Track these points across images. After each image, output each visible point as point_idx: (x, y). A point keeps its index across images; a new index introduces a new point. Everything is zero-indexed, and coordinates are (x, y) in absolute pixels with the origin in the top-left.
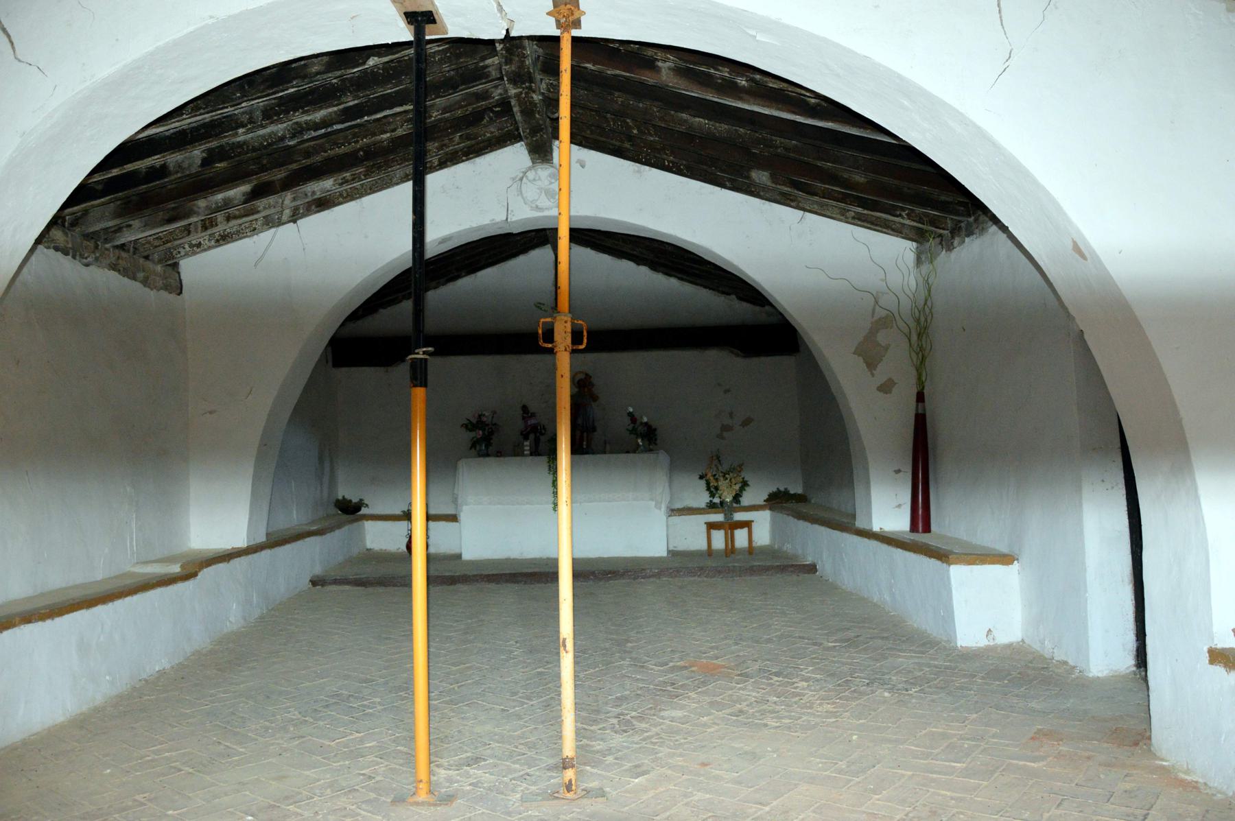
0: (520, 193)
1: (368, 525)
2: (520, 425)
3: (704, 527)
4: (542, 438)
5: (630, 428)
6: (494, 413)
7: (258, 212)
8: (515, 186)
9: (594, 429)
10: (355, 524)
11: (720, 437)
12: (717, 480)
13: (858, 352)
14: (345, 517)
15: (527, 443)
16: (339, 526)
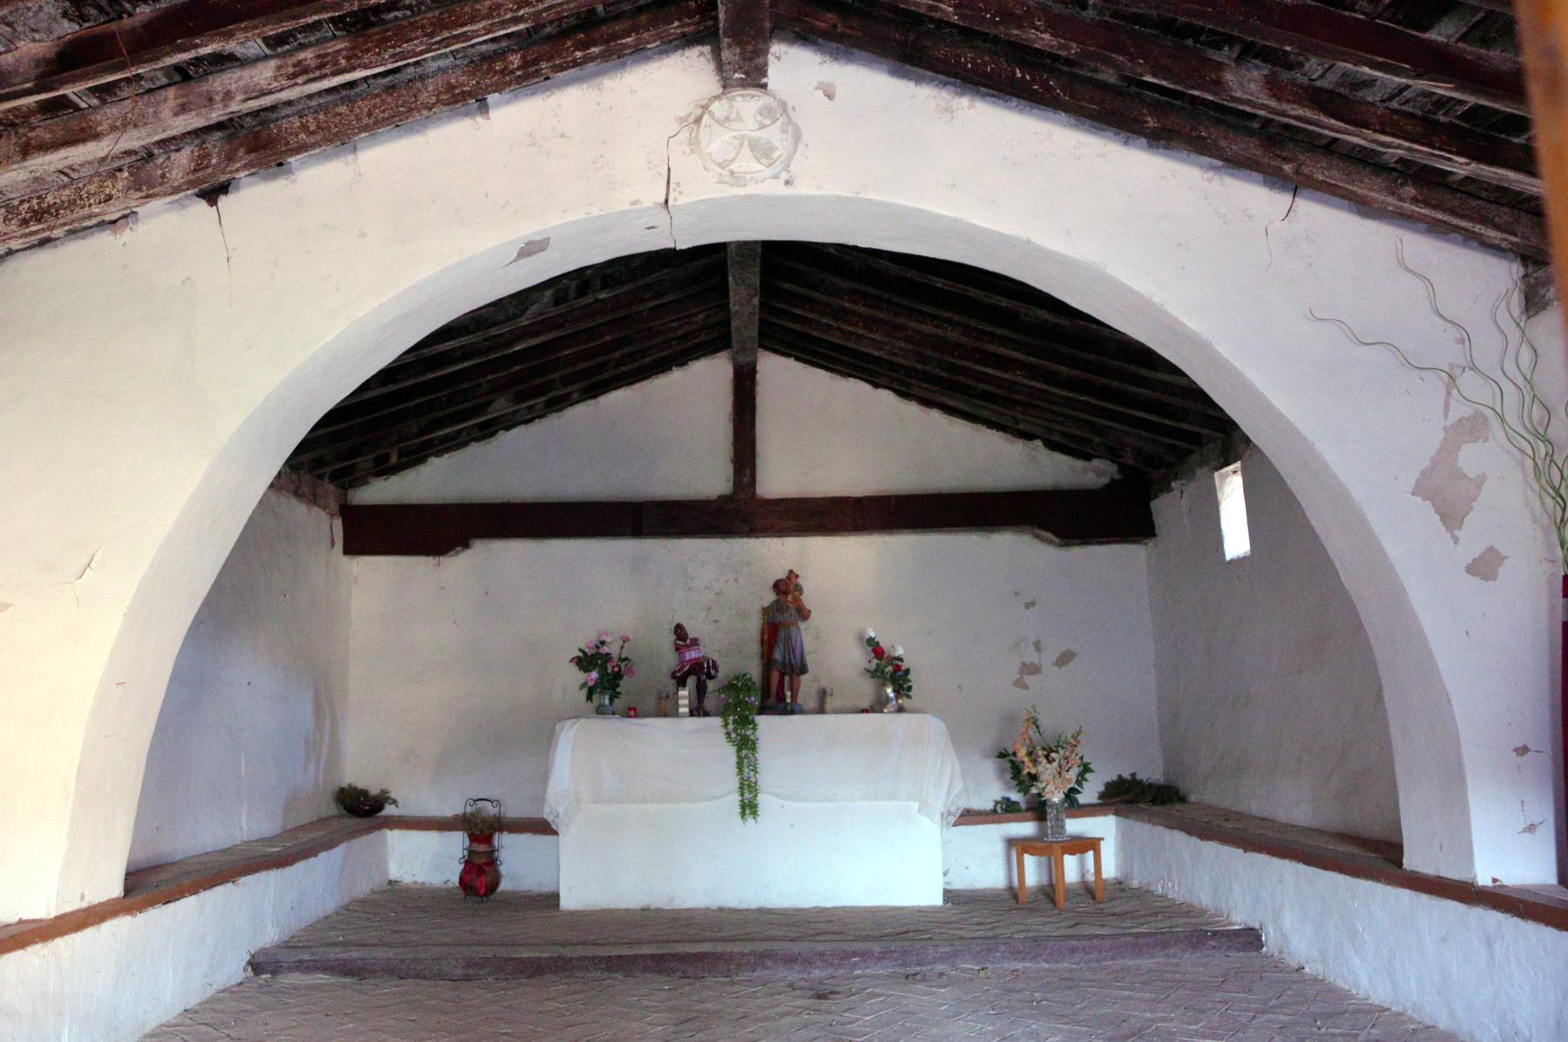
0: (694, 144)
1: (394, 837)
2: (670, 660)
3: (999, 849)
4: (711, 685)
5: (873, 666)
6: (626, 640)
7: (96, 136)
8: (684, 135)
9: (803, 669)
10: (365, 840)
11: (1020, 684)
12: (1035, 762)
15: (684, 693)
16: (329, 845)
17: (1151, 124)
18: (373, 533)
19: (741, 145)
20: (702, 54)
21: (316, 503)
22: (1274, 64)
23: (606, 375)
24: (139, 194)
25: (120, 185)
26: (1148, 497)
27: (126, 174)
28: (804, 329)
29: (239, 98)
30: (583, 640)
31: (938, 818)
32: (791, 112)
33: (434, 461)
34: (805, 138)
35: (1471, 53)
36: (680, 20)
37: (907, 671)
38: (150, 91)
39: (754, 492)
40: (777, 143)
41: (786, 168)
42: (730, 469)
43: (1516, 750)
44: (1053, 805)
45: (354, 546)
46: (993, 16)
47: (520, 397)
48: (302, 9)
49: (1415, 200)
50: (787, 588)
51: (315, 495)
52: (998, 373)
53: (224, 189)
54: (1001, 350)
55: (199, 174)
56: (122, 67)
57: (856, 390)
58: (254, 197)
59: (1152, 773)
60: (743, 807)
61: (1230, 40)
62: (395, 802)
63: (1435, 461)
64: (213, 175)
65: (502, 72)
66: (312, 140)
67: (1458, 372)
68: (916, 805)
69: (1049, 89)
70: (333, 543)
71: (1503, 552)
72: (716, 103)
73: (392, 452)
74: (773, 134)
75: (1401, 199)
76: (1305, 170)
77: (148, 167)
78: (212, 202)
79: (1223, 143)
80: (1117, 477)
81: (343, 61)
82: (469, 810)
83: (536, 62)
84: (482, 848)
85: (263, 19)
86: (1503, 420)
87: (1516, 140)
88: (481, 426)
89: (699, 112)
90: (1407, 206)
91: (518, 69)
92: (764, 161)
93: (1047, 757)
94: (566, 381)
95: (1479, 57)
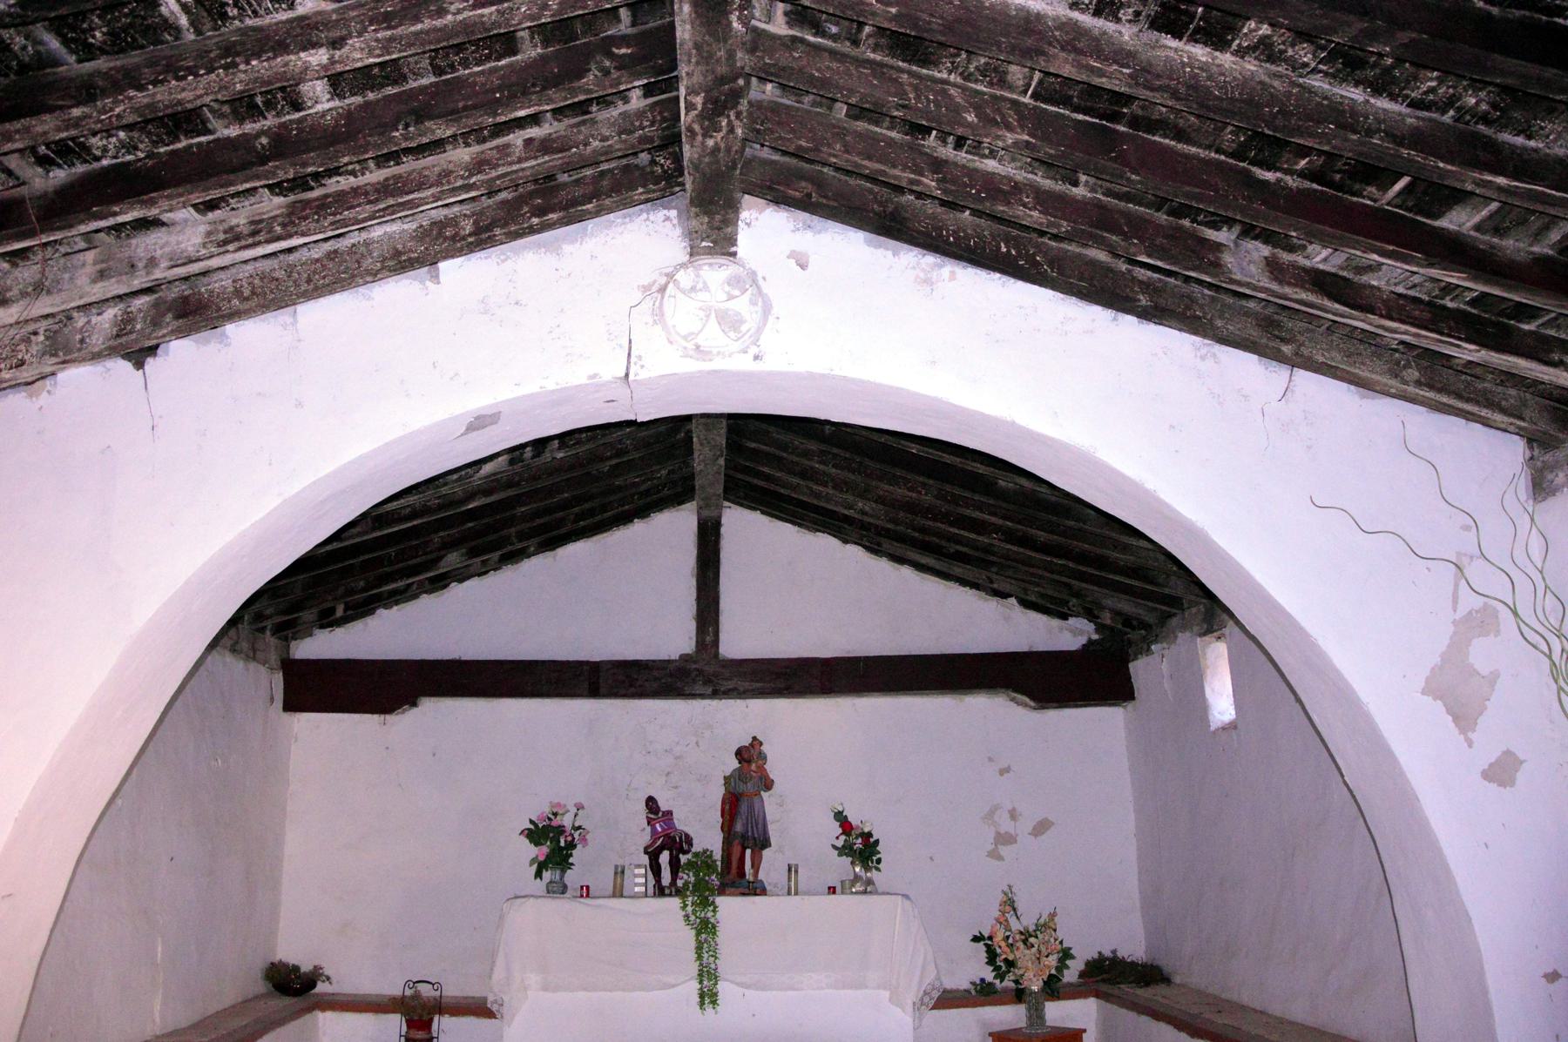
0: (659, 315)
1: (327, 1021)
5: (840, 843)
8: (647, 305)
9: (765, 843)
11: (995, 855)
13: (1433, 689)
14: (287, 1001)
17: (1144, 302)
18: (317, 688)
19: (708, 316)
20: (667, 219)
21: (254, 659)
22: (1274, 247)
23: (563, 531)
24: (54, 360)
25: (34, 349)
26: (1128, 662)
27: (41, 338)
28: (772, 487)
29: (164, 264)
30: (535, 809)
31: (910, 1008)
32: (761, 282)
33: (381, 612)
34: (775, 311)
35: (1484, 243)
36: (644, 186)
37: (877, 842)
38: (67, 254)
39: (717, 654)
40: (746, 316)
41: (755, 343)
42: (693, 626)
43: (1546, 976)
44: (1032, 992)
45: (294, 703)
46: (979, 192)
47: (473, 553)
48: (232, 177)
49: (1418, 383)
50: (749, 755)
51: (254, 651)
52: (973, 536)
53: (152, 350)
54: (977, 514)
55: (123, 340)
56: (31, 234)
57: (825, 543)
58: (182, 355)
59: (1134, 948)
60: (702, 996)
61: (1230, 222)
62: (328, 978)
63: (1445, 657)
64: (136, 340)
65: (454, 238)
66: (246, 306)
67: (1465, 561)
68: (887, 994)
69: (1036, 264)
70: (272, 699)
71: (1521, 756)
72: (682, 271)
73: (337, 615)
74: (741, 304)
75: (1406, 383)
76: (1305, 352)
77: (66, 331)
78: (139, 365)
79: (1219, 323)
80: (1095, 637)
81: (278, 228)
82: (408, 992)
83: (489, 228)
84: (420, 1035)
85: (188, 187)
86: (1515, 613)
87: (1526, 327)
88: (433, 580)
89: (663, 280)
90: (1411, 389)
91: (470, 235)
92: (732, 334)
93: (1025, 942)
94: (522, 536)
95: (1492, 247)
